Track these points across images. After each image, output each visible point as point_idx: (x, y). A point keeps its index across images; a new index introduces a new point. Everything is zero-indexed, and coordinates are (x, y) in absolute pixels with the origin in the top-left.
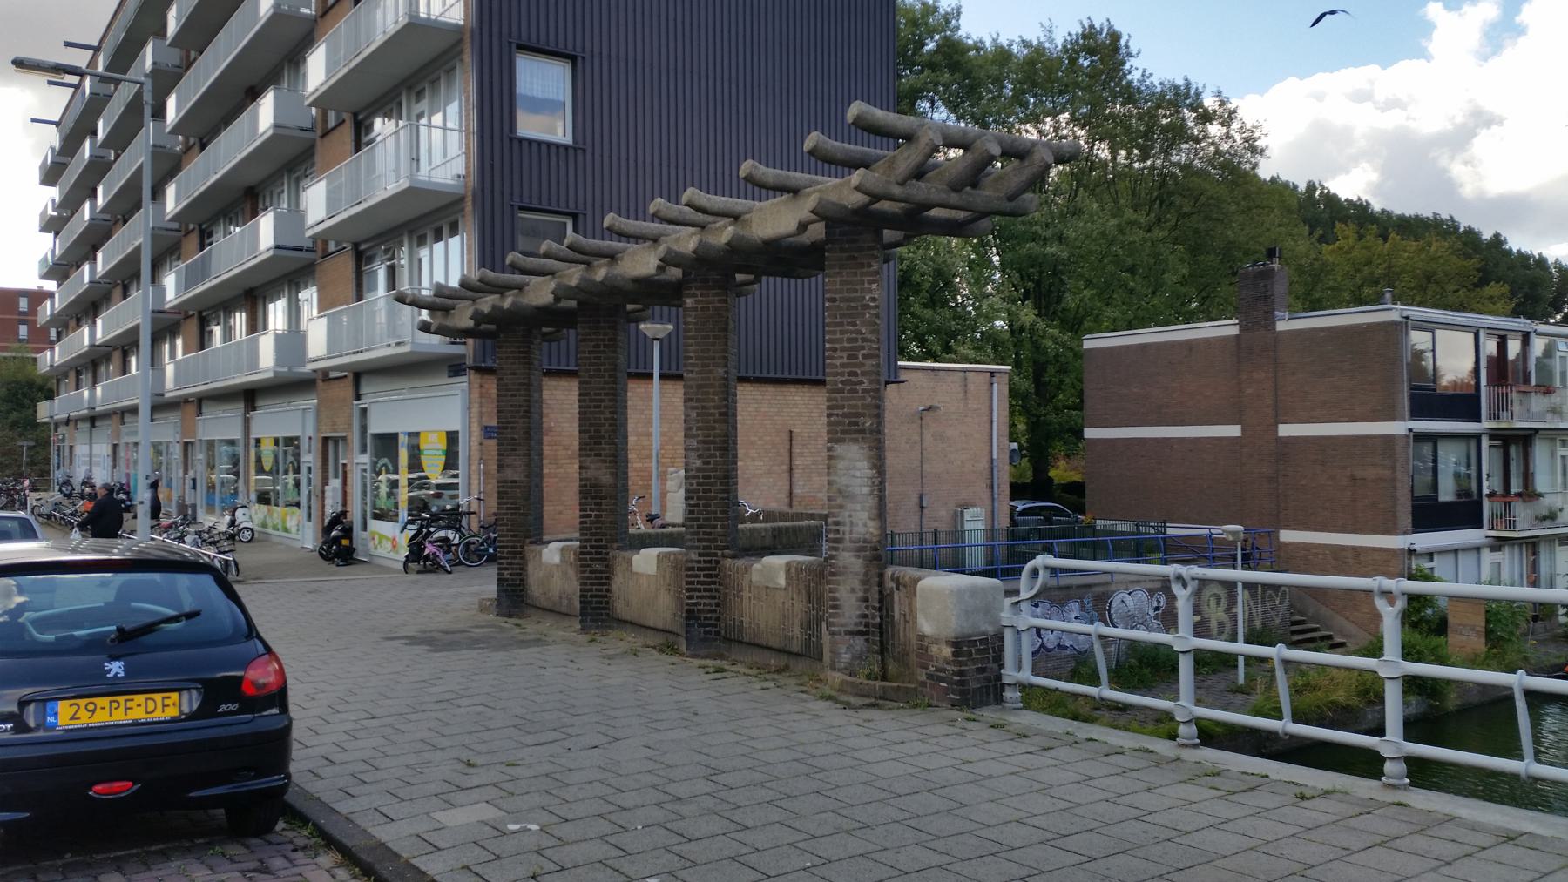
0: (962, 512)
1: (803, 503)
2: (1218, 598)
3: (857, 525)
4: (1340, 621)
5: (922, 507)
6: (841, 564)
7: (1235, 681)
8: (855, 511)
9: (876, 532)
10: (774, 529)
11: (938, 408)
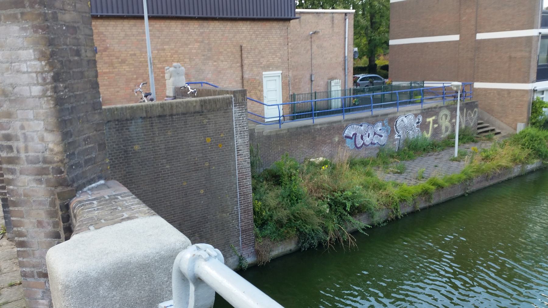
0: (330, 82)
1: (249, 82)
2: (446, 116)
3: (33, 139)
4: (498, 123)
5: (312, 81)
6: (21, 191)
7: (453, 154)
8: (27, 120)
9: (57, 149)
10: (201, 101)
11: (318, 32)
